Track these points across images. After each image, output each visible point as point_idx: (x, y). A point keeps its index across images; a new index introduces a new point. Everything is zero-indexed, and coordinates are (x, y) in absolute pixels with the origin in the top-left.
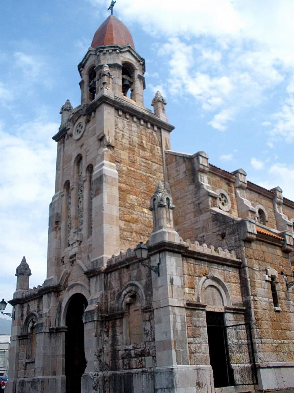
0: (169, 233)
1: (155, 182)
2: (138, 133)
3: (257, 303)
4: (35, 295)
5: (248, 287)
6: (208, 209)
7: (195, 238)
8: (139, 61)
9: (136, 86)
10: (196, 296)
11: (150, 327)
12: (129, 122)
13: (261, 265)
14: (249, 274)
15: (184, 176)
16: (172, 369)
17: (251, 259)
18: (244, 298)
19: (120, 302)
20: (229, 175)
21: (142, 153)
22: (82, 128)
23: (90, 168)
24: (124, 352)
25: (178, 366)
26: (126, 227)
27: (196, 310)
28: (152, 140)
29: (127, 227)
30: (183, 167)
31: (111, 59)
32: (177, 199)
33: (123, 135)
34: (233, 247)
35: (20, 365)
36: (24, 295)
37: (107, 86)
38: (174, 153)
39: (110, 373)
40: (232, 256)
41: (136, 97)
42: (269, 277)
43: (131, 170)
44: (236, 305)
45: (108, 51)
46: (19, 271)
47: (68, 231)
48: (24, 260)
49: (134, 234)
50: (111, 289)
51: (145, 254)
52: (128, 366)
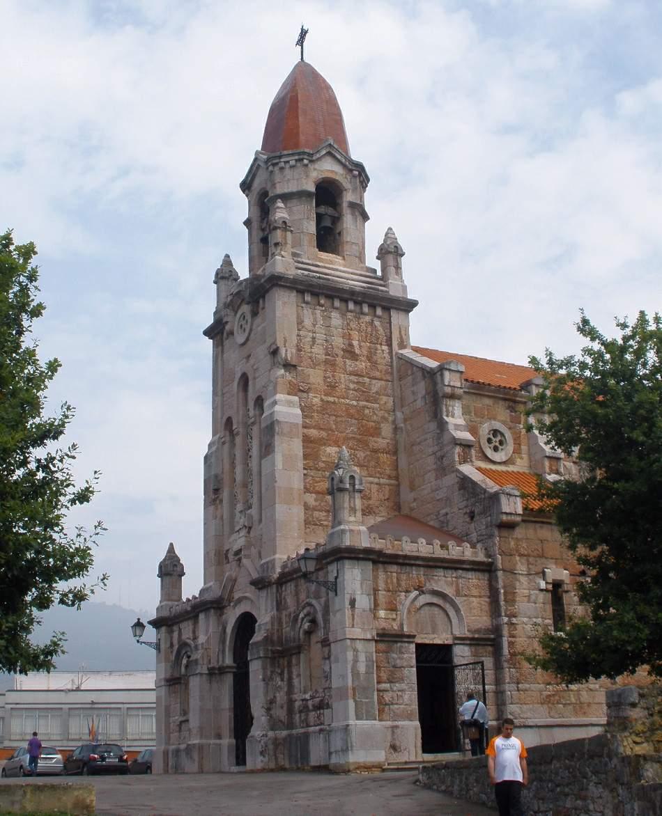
0: (351, 531)
1: (377, 416)
2: (342, 329)
3: (515, 628)
4: (187, 612)
5: (499, 604)
6: (453, 467)
7: (436, 516)
8: (351, 171)
9: (345, 226)
10: (399, 623)
12: (325, 311)
13: (532, 564)
14: (504, 582)
15: (423, 404)
16: (348, 725)
17: (511, 555)
18: (494, 620)
19: (297, 629)
21: (350, 366)
23: (259, 401)
24: (301, 702)
25: (359, 722)
26: (317, 504)
27: (396, 642)
28: (371, 335)
29: (320, 504)
30: (421, 388)
31: (293, 179)
32: (413, 445)
33: (314, 338)
34: (483, 535)
35: (172, 725)
36: (173, 611)
37: (281, 250)
38: (409, 358)
39: (285, 733)
40: (475, 554)
41: (345, 248)
42: (547, 583)
43: (328, 402)
44: (478, 631)
45: (288, 162)
46: (163, 568)
47: (233, 505)
50: (286, 608)
51: (311, 566)
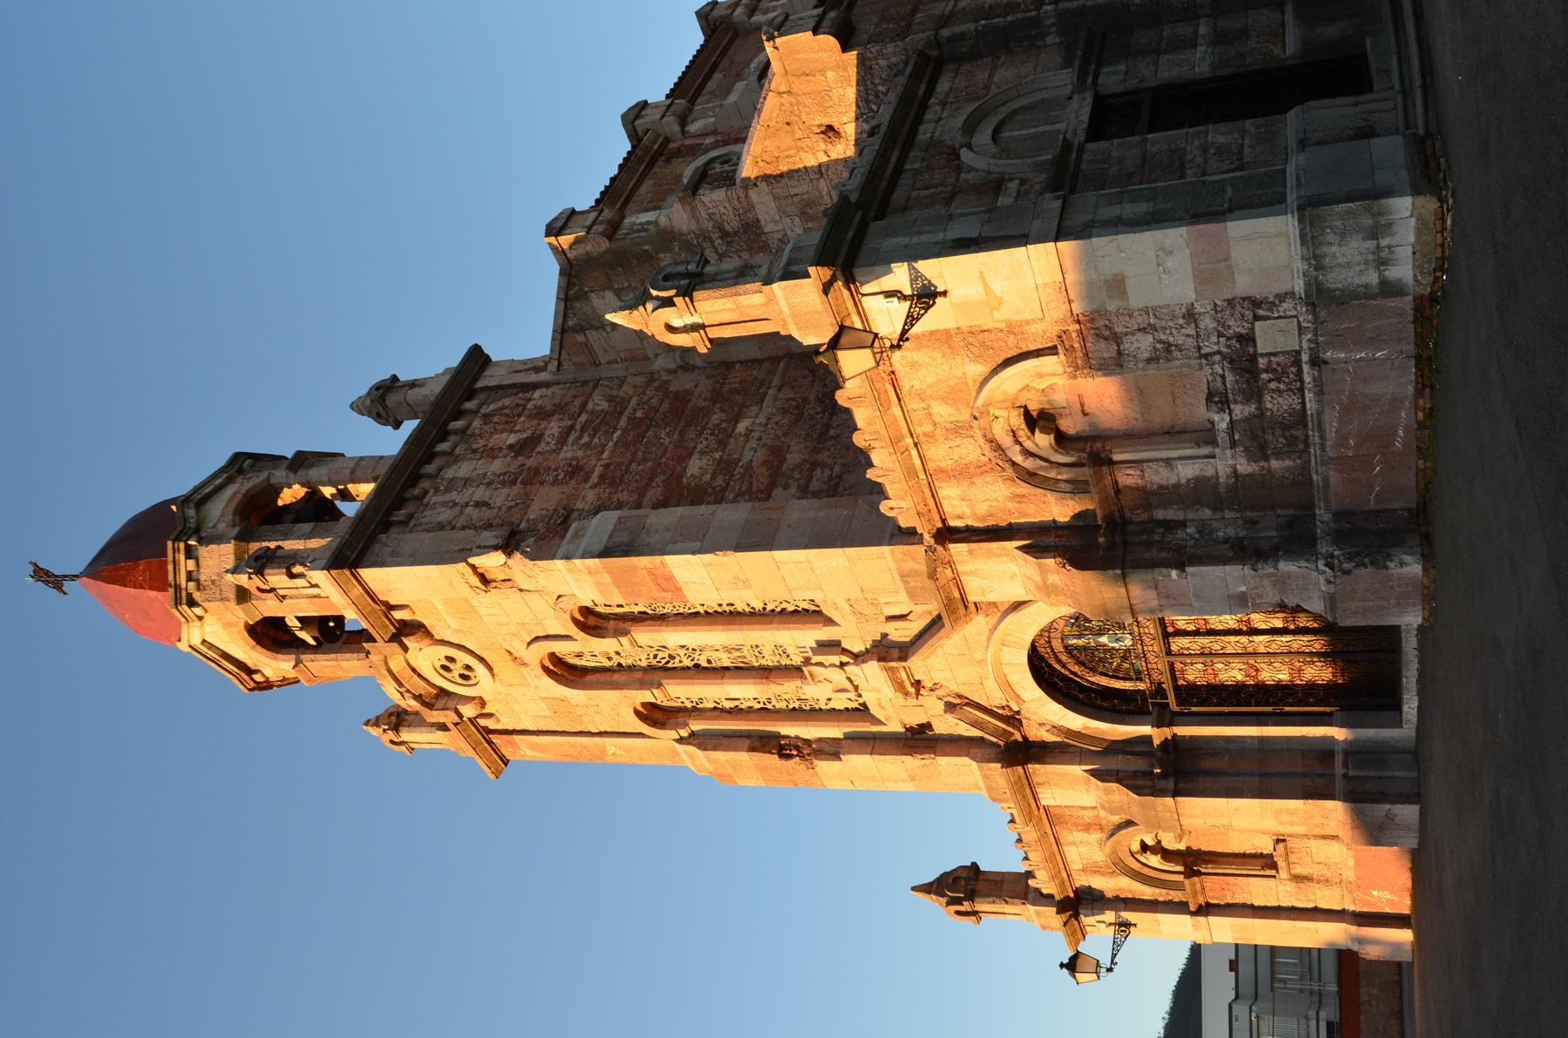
11: (1140, 335)
20: (638, 152)
22: (451, 659)
43: (601, 477)
48: (926, 889)
49: (823, 457)
52: (1294, 432)
